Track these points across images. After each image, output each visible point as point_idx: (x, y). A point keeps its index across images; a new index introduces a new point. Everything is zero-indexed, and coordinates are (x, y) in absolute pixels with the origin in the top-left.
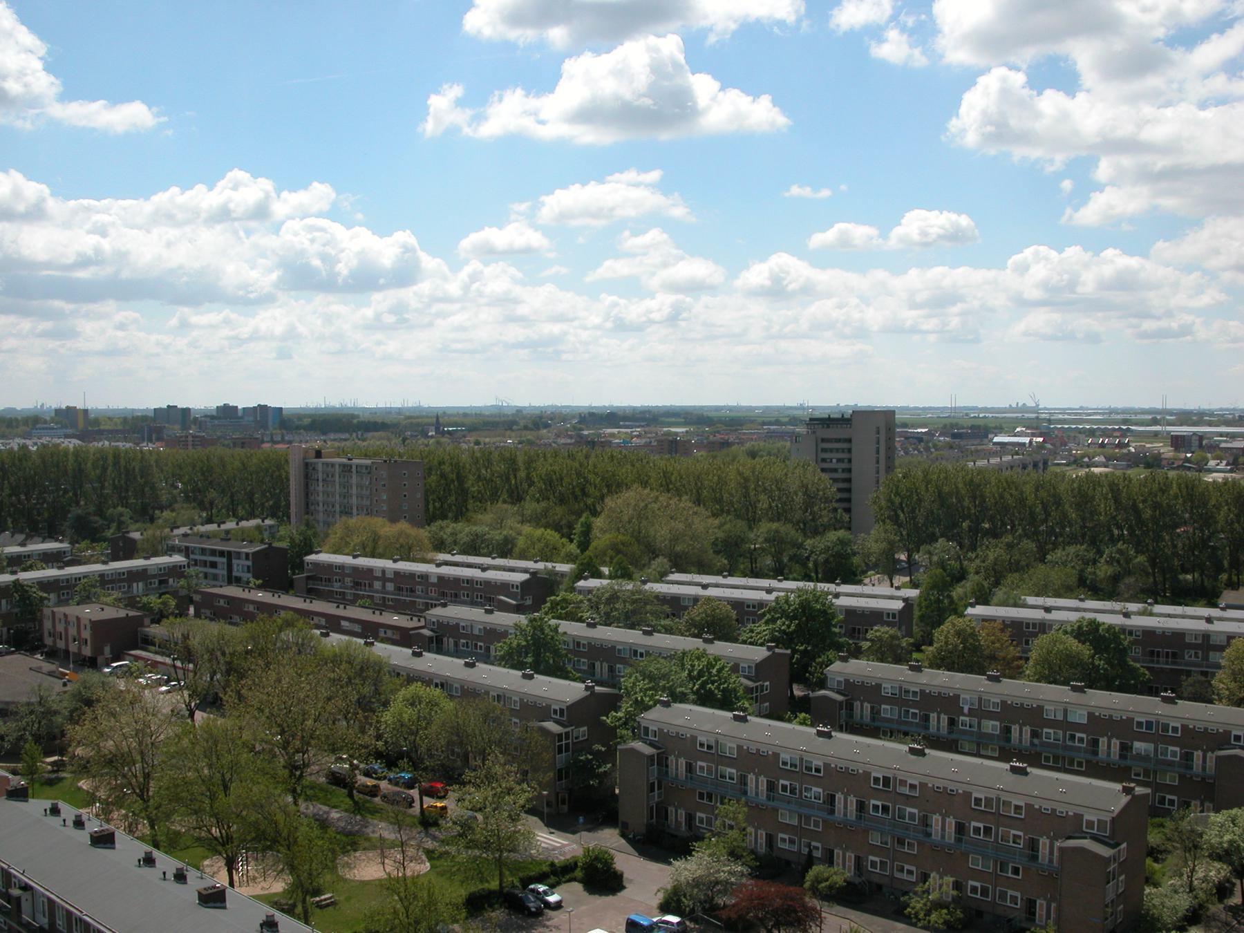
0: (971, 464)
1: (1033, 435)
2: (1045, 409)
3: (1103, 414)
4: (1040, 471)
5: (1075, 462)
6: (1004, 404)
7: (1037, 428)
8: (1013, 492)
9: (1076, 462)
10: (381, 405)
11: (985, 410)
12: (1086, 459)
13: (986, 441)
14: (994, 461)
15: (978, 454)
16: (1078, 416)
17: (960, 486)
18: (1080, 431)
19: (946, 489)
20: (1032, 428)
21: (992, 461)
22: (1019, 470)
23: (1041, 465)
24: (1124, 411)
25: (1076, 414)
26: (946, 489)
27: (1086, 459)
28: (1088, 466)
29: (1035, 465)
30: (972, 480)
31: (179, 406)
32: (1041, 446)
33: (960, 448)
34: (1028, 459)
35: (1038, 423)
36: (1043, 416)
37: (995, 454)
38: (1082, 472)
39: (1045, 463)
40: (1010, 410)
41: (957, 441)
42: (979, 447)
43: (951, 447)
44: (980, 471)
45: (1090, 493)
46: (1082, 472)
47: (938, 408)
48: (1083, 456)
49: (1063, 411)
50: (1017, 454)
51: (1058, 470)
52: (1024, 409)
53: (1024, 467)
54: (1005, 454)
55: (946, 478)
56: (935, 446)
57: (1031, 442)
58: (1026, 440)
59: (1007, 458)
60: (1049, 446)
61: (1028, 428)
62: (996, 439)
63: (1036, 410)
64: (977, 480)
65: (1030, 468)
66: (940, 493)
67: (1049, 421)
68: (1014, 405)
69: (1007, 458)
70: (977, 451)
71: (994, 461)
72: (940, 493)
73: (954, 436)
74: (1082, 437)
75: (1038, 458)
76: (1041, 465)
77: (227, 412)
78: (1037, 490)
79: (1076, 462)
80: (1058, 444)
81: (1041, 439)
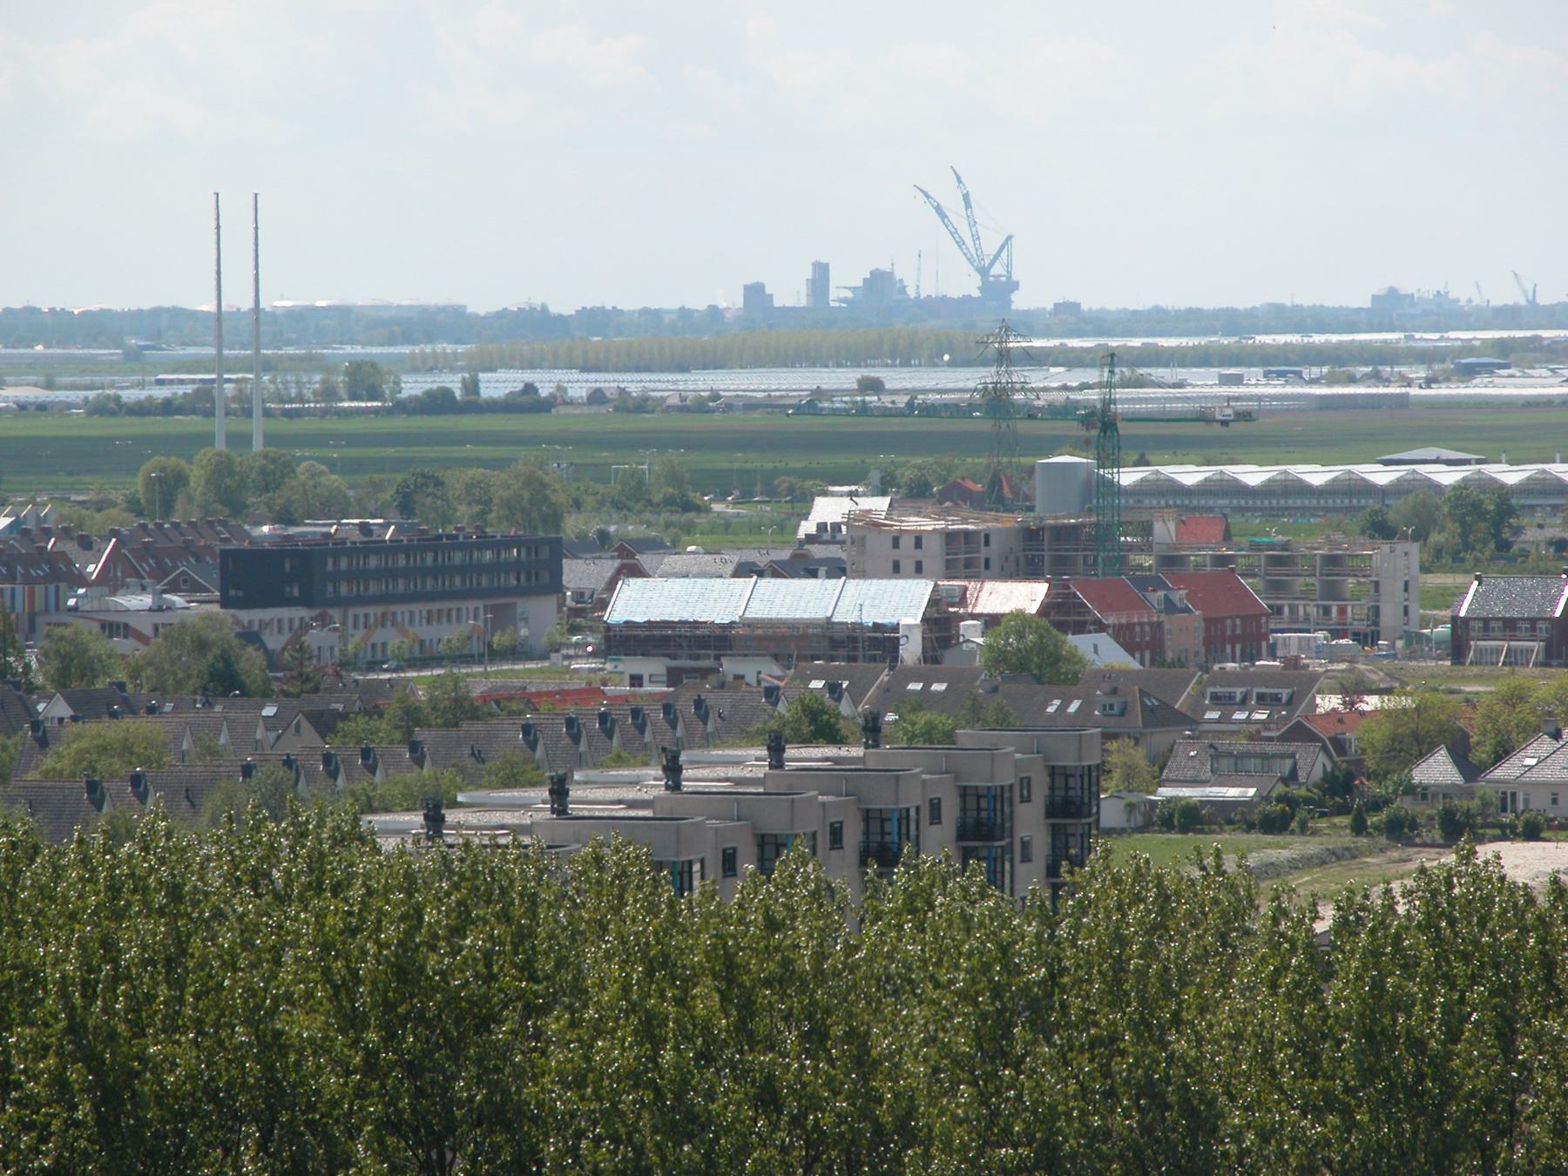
0: (397, 829)
1: (966, 558)
2: (1069, 317)
3: (1278, 362)
4: (1031, 881)
5: (1339, 791)
6: (691, 277)
7: (995, 496)
8: (792, 1064)
9: (1350, 793)
10: (1112, 307)
11: (531, 335)
12: (1437, 769)
13: (538, 617)
14: (614, 791)
15: (465, 737)
16: (1357, 383)
17: (301, 1026)
18: (1380, 517)
19: (174, 1059)
20: (954, 495)
21: (595, 794)
22: (842, 872)
23: (1030, 822)
24: (1507, 315)
25: (1338, 361)
26: (174, 1059)
27: (1437, 769)
28: (1458, 827)
29: (982, 829)
30: (405, 971)
31: (145, 308)
32: (1031, 657)
33: (299, 678)
34: (919, 778)
35: (1004, 448)
36: (1048, 383)
37: (614, 731)
38: (1396, 879)
39: (1071, 805)
40: (759, 332)
41: (277, 623)
42: (479, 680)
43: (224, 681)
44: (480, 884)
45: (1474, 1064)
46: (1396, 879)
47: (97, 327)
48: (1413, 741)
49: (1229, 339)
50: (824, 729)
51: (1169, 855)
52: (881, 322)
53: (881, 851)
54: (717, 728)
55: (173, 962)
56: (73, 671)
57: (941, 624)
58: (898, 602)
59: (727, 768)
60: (1100, 651)
61: (915, 494)
62: (638, 602)
63: (987, 329)
64: (447, 968)
65: (936, 847)
66: (113, 1093)
67: (1105, 431)
68: (789, 292)
69: (727, 768)
70: (459, 710)
71: (614, 791)
72: (113, 1093)
73: (254, 577)
74: (1396, 561)
75: (1007, 759)
76: (1030, 822)
77: (684, 313)
78: (994, 1043)
79: (1350, 793)
80: (1185, 633)
81: (1026, 596)
